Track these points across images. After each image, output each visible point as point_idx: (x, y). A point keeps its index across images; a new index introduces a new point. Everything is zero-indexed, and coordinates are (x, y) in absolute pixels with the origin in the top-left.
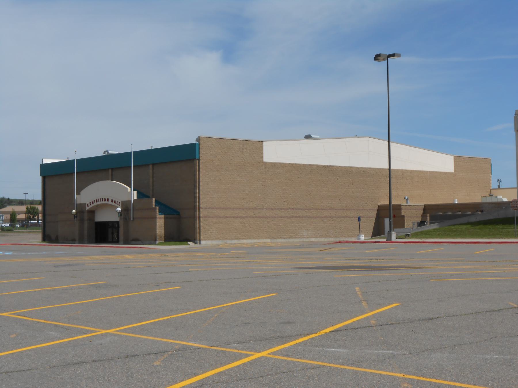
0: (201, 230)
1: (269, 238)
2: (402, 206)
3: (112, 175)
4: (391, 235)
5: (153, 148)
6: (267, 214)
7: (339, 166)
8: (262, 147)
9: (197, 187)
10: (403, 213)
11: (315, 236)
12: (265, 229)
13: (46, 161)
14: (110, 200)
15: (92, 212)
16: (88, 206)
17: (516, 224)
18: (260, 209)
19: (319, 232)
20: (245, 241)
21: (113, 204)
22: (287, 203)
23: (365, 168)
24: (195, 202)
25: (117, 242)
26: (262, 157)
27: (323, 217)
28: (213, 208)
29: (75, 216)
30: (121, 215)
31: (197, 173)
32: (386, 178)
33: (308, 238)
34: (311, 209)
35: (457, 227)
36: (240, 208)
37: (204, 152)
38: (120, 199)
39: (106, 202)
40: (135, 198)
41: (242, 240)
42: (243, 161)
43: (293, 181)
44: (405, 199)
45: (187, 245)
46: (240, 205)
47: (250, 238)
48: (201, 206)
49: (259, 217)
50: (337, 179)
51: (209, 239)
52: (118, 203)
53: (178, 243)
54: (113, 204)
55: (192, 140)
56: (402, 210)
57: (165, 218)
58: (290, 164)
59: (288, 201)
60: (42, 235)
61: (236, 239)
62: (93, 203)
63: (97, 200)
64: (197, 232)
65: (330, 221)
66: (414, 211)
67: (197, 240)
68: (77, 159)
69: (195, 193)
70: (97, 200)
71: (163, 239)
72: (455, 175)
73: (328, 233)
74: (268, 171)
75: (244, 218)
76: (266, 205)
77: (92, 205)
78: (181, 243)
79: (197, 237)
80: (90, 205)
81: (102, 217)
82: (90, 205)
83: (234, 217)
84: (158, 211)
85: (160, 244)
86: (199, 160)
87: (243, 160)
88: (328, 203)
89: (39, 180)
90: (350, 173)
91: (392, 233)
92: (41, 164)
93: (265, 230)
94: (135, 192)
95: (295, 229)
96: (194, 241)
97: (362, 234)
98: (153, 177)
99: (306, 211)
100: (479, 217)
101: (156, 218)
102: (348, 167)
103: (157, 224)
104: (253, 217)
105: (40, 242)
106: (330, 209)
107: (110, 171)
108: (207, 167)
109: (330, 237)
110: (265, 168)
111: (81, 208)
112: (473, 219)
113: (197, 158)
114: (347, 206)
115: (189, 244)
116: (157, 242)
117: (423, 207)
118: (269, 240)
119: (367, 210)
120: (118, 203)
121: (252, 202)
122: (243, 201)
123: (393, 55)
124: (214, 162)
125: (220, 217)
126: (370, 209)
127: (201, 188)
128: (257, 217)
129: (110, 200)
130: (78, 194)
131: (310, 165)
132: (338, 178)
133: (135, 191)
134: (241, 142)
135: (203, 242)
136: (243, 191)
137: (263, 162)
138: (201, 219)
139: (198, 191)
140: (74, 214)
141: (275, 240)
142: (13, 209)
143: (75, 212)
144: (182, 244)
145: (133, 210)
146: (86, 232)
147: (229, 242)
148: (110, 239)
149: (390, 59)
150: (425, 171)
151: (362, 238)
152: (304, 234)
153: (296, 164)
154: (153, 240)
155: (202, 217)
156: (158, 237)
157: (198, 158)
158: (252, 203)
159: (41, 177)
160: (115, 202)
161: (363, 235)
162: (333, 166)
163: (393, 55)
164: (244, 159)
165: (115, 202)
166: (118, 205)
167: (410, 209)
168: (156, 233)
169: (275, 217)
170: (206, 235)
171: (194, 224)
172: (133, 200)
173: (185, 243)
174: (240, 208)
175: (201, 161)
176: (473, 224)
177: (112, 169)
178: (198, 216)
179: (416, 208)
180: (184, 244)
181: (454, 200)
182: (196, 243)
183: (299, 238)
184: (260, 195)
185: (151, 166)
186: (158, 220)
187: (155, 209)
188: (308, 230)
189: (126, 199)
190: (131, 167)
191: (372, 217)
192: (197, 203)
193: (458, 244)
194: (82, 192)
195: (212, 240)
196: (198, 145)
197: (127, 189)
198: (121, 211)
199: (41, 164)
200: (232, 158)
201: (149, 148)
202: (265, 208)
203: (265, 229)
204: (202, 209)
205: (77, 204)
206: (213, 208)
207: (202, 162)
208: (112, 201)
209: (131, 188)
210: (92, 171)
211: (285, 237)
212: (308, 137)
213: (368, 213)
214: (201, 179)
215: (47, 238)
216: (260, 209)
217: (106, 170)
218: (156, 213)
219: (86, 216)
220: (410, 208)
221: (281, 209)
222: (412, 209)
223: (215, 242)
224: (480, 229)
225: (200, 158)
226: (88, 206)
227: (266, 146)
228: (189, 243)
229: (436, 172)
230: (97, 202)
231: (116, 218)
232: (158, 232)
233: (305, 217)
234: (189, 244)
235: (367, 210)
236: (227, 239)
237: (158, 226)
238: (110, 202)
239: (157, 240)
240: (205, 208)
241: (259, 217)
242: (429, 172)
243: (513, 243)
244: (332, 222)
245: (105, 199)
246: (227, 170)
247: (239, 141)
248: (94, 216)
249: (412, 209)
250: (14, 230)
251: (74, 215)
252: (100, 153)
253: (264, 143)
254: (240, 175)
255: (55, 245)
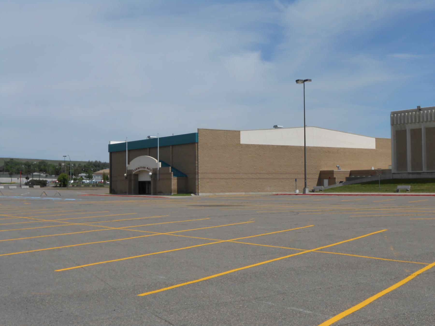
0: (199, 187)
1: (244, 192)
2: (334, 172)
3: (149, 152)
4: (305, 190)
5: (174, 135)
6: (242, 177)
7: (293, 146)
8: (240, 135)
9: (197, 160)
10: (335, 176)
11: (275, 191)
12: (241, 186)
13: (112, 143)
14: (146, 168)
15: (136, 175)
16: (134, 171)
17: (380, 184)
18: (238, 173)
19: (278, 188)
20: (228, 194)
21: (148, 170)
22: (256, 170)
23: (311, 147)
24: (196, 169)
25: (149, 194)
26: (240, 141)
27: (281, 179)
28: (207, 173)
29: (126, 178)
30: (152, 177)
31: (197, 151)
32: (326, 153)
33: (270, 192)
34: (273, 174)
35: (353, 185)
36: (225, 173)
37: (201, 138)
38: (152, 167)
39: (144, 169)
40: (160, 166)
41: (226, 193)
42: (226, 144)
43: (260, 156)
44: (337, 167)
45: (190, 195)
46: (225, 171)
47: (231, 192)
48: (199, 172)
49: (237, 179)
50: (291, 154)
51: (204, 192)
52: (151, 170)
53: (185, 194)
54: (148, 170)
55: (193, 130)
56: (334, 174)
57: (178, 179)
58: (258, 145)
59: (257, 168)
60: (110, 190)
61: (222, 192)
62: (136, 170)
63: (139, 168)
64: (196, 188)
65: (286, 181)
66: (343, 174)
67: (196, 193)
68: (128, 142)
69: (195, 164)
70: (139, 168)
71: (177, 192)
72: (376, 151)
73: (284, 189)
74: (243, 149)
75: (227, 179)
76: (242, 171)
77: (136, 171)
78: (187, 194)
79: (196, 191)
80: (135, 171)
81: (143, 178)
82: (135, 171)
83: (220, 179)
84: (172, 174)
85: (174, 195)
86: (198, 143)
87: (227, 143)
88: (285, 170)
89: (108, 154)
90: (300, 150)
91: (306, 189)
92: (109, 145)
93: (242, 186)
94: (160, 163)
95: (262, 186)
96: (195, 193)
97: (297, 189)
98: (172, 154)
99: (269, 174)
100: (370, 178)
101: (171, 179)
102: (299, 146)
103: (172, 183)
104: (233, 179)
105: (108, 194)
106: (286, 173)
107: (148, 149)
108: (203, 148)
109: (286, 191)
110: (242, 148)
111: (130, 173)
112: (365, 180)
113: (197, 142)
114: (298, 172)
115: (191, 195)
116: (172, 194)
117: (350, 172)
118: (244, 193)
119: (312, 174)
120: (151, 170)
121: (233, 169)
122: (226, 168)
123: (306, 80)
124: (208, 144)
125: (211, 179)
126: (314, 174)
127: (199, 161)
128: (236, 179)
129: (146, 168)
130: (129, 164)
131: (272, 145)
132: (292, 153)
133: (160, 162)
134: (226, 131)
135: (200, 194)
136: (227, 162)
137: (240, 144)
138: (199, 180)
139: (197, 162)
140: (126, 176)
141: (248, 193)
142: (104, 171)
143: (126, 175)
144: (186, 195)
145: (159, 174)
146: (133, 187)
147: (217, 194)
148: (147, 192)
149: (305, 83)
150: (354, 149)
151: (297, 191)
152: (268, 189)
153: (262, 145)
154: (169, 193)
155: (200, 179)
156: (172, 191)
157: (197, 142)
158: (232, 170)
159: (109, 153)
160: (149, 169)
161: (298, 190)
162: (288, 146)
163: (306, 80)
164: (227, 142)
165: (149, 169)
166: (150, 171)
167: (340, 174)
168: (171, 189)
169: (248, 179)
170: (202, 189)
171: (195, 183)
172: (159, 168)
173: (189, 194)
174: (225, 173)
175: (199, 144)
176: (363, 183)
177: (150, 148)
178: (197, 178)
179: (344, 172)
180: (188, 195)
181: (371, 168)
182: (196, 195)
183: (264, 192)
184: (238, 165)
185: (171, 147)
186: (172, 181)
187: (171, 173)
188: (270, 187)
189: (154, 167)
190: (158, 147)
191: (316, 179)
192: (196, 170)
193: (340, 196)
194: (131, 163)
195: (206, 192)
196: (197, 134)
197: (156, 161)
198: (152, 175)
199: (109, 145)
200: (219, 142)
201: (171, 135)
202: (241, 173)
203: (241, 186)
204: (200, 173)
205: (127, 170)
206: (207, 173)
207: (200, 145)
208: (147, 168)
209: (157, 160)
210: (138, 149)
211: (255, 191)
212: (276, 127)
213: (313, 176)
214: (199, 155)
215: (113, 191)
216: (238, 173)
217: (146, 149)
218: (171, 176)
219: (133, 178)
220: (340, 173)
221: (252, 173)
222: (342, 173)
223: (208, 194)
224: (365, 186)
225: (199, 142)
226: (134, 171)
227: (242, 133)
228: (192, 194)
229: (362, 149)
230: (139, 169)
231: (148, 179)
232: (172, 187)
233: (269, 179)
234: (191, 195)
235: (312, 174)
236: (216, 192)
237: (172, 184)
238: (146, 169)
239: (172, 192)
240: (202, 173)
241: (237, 179)
242: (357, 149)
243: (369, 195)
244: (288, 182)
245: (143, 167)
246: (216, 149)
247: (224, 131)
248: (138, 178)
249: (342, 173)
250: (105, 186)
251: (126, 177)
252: (145, 138)
253: (241, 132)
254: (225, 152)
255: (113, 196)
